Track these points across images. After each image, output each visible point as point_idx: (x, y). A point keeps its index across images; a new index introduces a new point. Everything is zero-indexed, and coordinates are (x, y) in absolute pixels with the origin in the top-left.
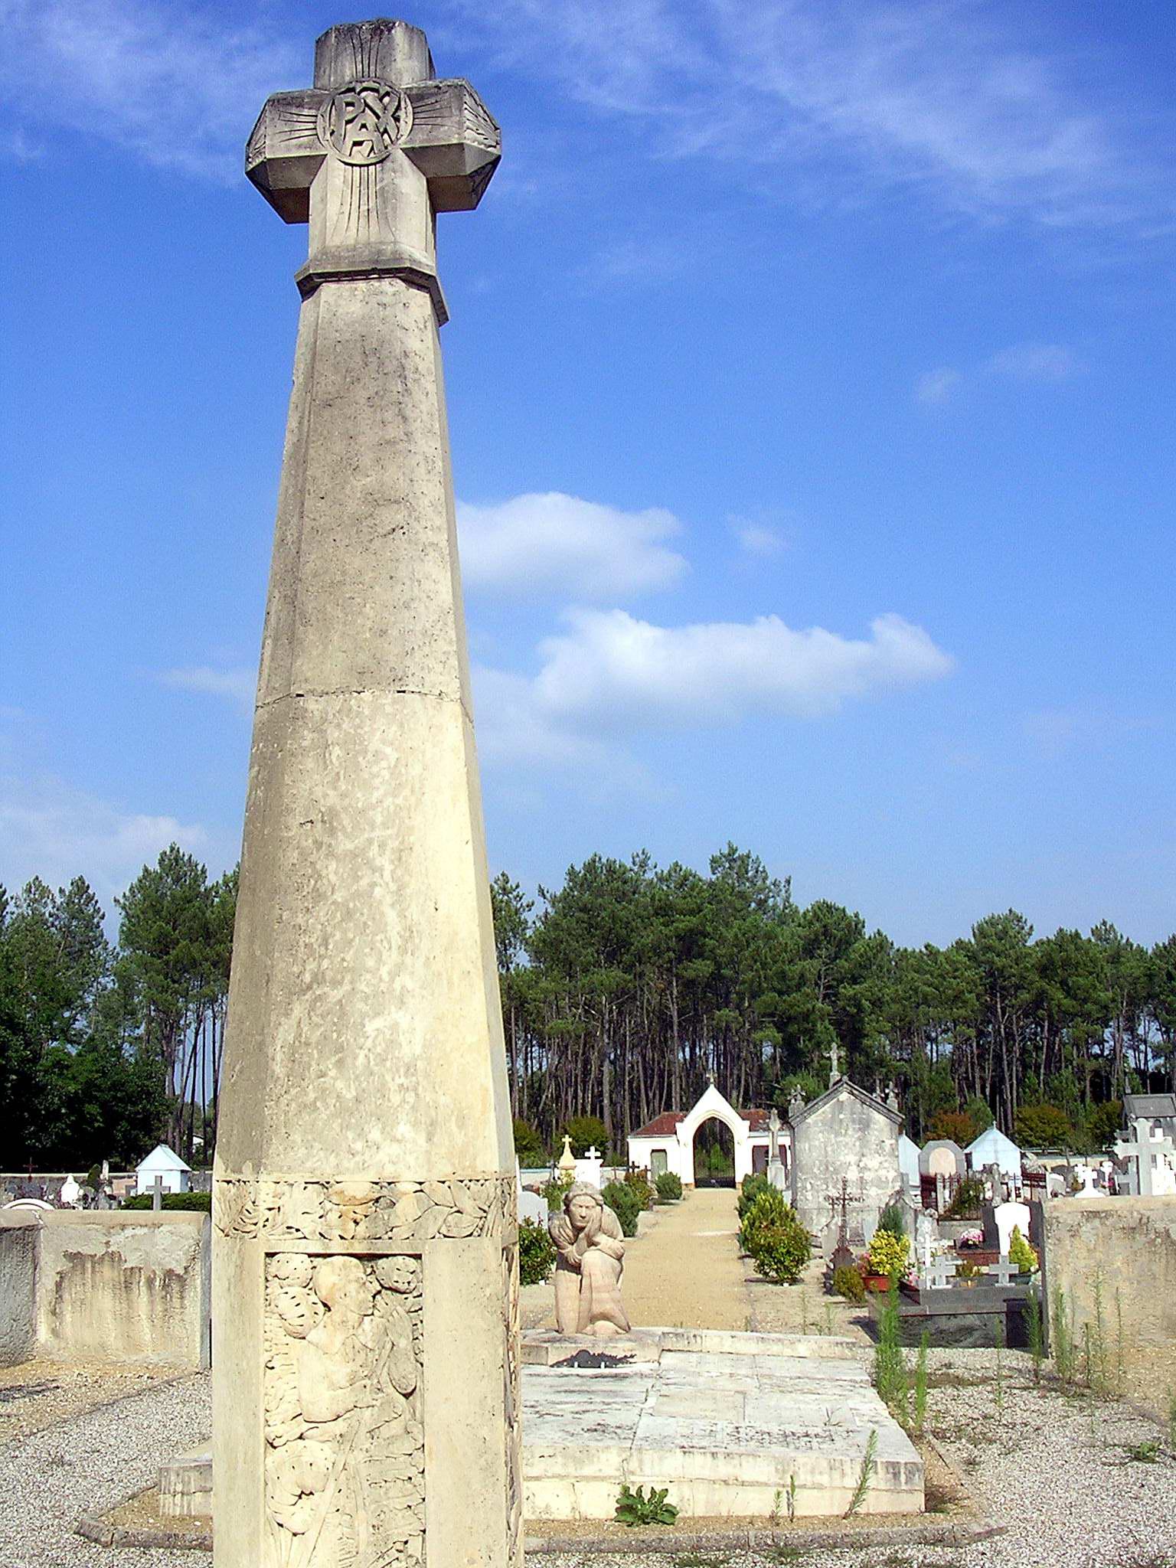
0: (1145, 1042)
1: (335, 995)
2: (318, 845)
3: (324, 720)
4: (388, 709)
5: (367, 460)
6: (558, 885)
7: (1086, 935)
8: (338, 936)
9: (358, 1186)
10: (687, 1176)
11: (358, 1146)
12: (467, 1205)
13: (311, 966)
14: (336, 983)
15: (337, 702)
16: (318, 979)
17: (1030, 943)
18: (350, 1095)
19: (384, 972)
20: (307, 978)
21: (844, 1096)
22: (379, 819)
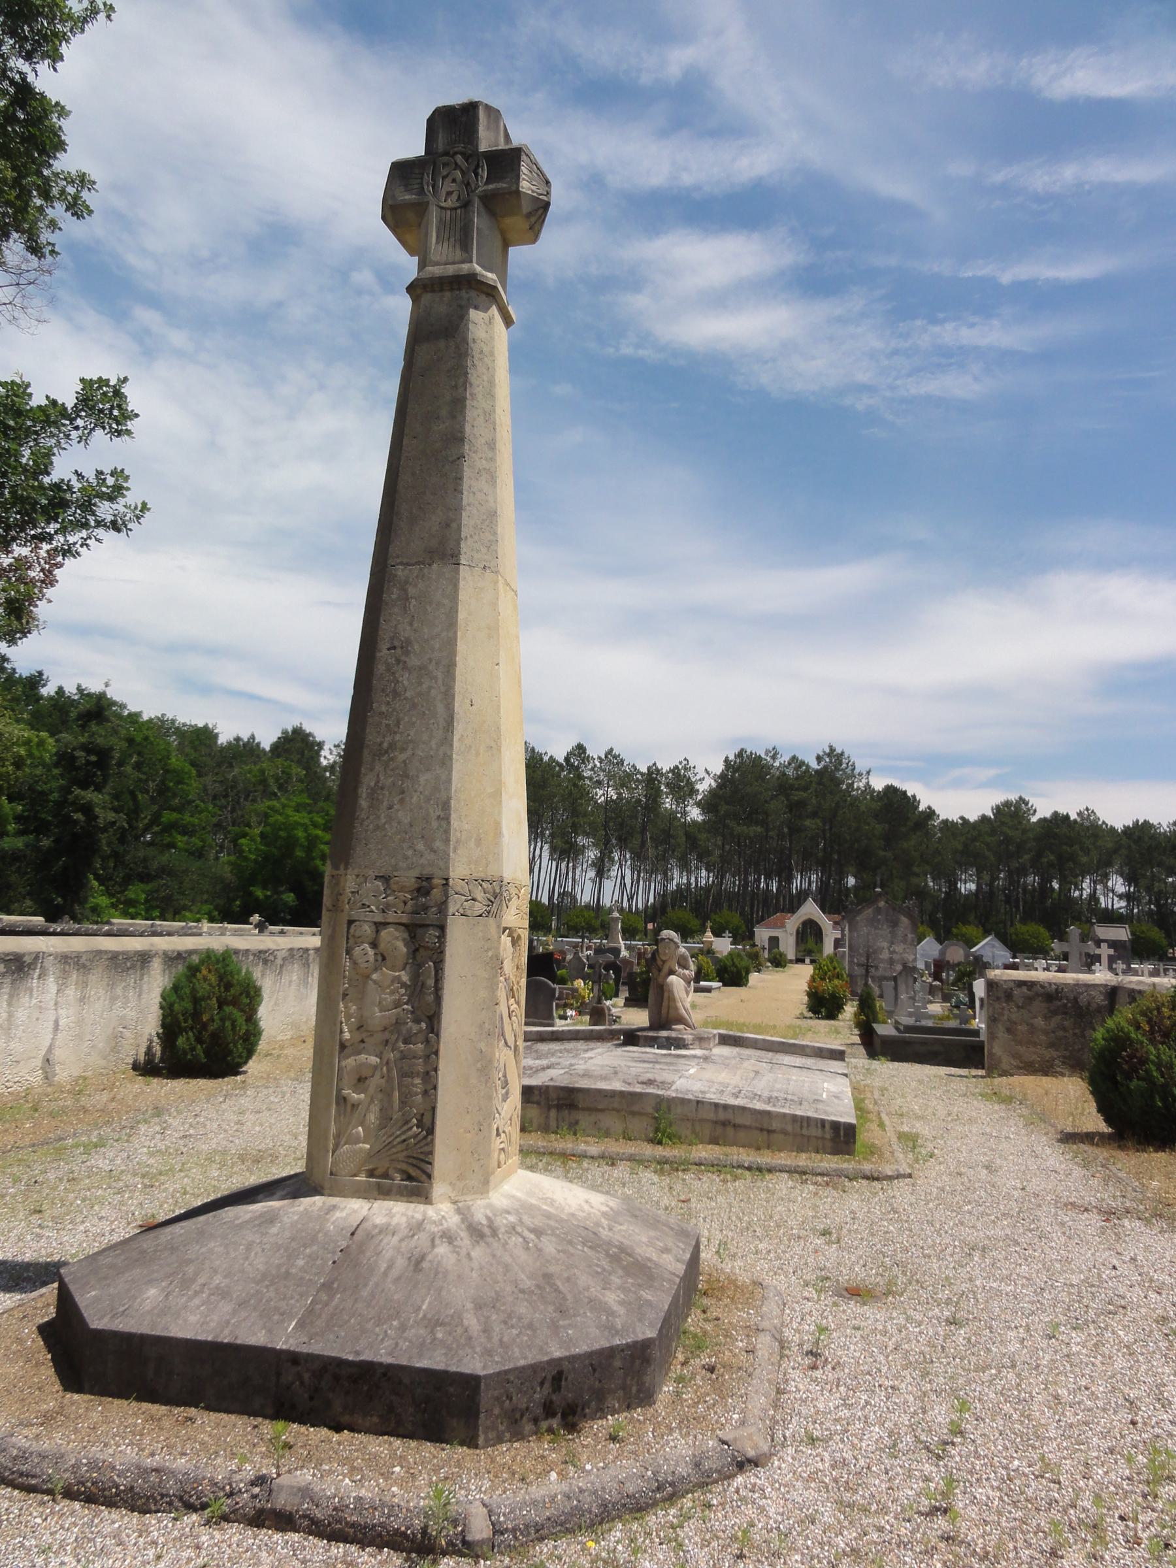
0: (1113, 891)
1: (402, 757)
2: (398, 661)
3: (406, 582)
4: (447, 575)
5: (444, 412)
6: (718, 768)
7: (1073, 816)
8: (406, 719)
9: (408, 878)
10: (791, 955)
11: (410, 853)
12: (479, 895)
13: (388, 739)
14: (403, 750)
15: (416, 569)
16: (392, 746)
17: (1034, 819)
18: (406, 821)
19: (433, 744)
20: (385, 745)
21: (882, 904)
22: (437, 646)
